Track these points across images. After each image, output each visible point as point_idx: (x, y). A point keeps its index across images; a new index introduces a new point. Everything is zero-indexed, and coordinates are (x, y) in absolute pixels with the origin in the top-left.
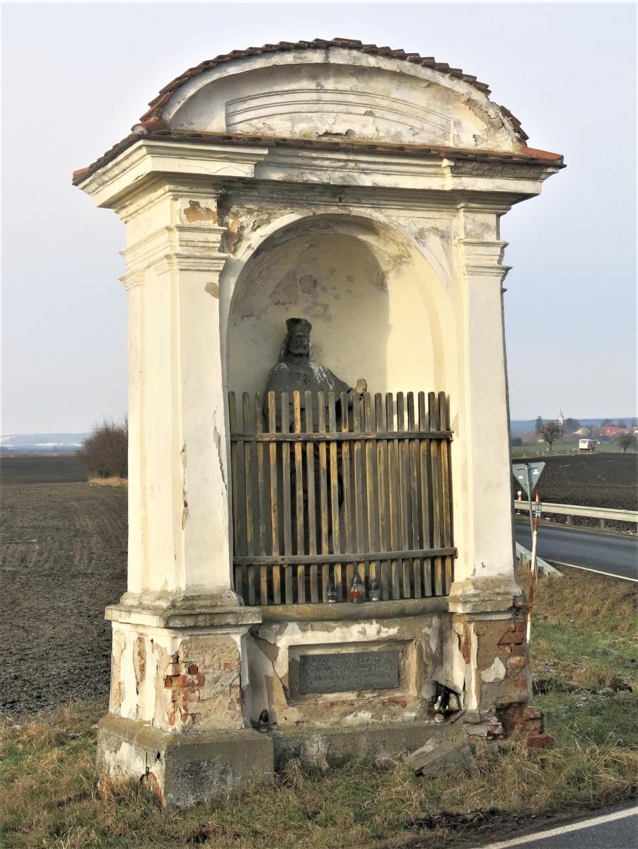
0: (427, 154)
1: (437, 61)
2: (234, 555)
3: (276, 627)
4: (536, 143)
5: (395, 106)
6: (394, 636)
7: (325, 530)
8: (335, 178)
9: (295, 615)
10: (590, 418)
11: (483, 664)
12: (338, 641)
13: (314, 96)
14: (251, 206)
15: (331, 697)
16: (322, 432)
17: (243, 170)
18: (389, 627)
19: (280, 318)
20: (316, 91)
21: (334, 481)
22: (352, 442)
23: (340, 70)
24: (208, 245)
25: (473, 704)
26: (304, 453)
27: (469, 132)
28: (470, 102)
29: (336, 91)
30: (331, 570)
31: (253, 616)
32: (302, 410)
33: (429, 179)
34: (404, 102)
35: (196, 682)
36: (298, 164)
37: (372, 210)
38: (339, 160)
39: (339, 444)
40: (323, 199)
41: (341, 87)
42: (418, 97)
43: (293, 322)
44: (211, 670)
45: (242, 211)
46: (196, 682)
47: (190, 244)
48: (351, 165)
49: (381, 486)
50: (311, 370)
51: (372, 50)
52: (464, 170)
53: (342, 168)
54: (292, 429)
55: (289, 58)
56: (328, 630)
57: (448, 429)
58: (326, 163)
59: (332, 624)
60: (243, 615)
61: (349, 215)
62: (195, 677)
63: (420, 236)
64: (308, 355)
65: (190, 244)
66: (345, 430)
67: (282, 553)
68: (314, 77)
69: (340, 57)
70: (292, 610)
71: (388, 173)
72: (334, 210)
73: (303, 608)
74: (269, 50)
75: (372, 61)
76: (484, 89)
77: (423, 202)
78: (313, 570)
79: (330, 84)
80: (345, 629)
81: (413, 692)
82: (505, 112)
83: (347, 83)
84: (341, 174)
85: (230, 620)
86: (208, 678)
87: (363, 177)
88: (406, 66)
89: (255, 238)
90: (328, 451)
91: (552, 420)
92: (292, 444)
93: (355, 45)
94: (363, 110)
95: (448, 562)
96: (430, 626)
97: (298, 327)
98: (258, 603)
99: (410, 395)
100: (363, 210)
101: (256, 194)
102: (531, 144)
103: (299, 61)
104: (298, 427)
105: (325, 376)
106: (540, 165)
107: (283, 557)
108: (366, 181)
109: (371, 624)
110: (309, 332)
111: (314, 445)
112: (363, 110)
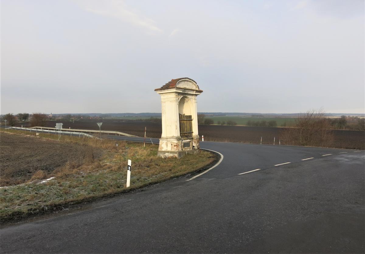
0: (194, 90)
4: (201, 89)
10: (208, 112)
11: (197, 144)
23: (188, 81)
25: (196, 148)
27: (194, 88)
28: (195, 85)
33: (166, 96)
42: (191, 84)
63: (191, 99)
69: (187, 79)
76: (196, 83)
79: (185, 82)
81: (191, 147)
82: (198, 86)
83: (186, 82)
89: (180, 98)
102: (200, 89)
106: (201, 92)
108: (189, 93)
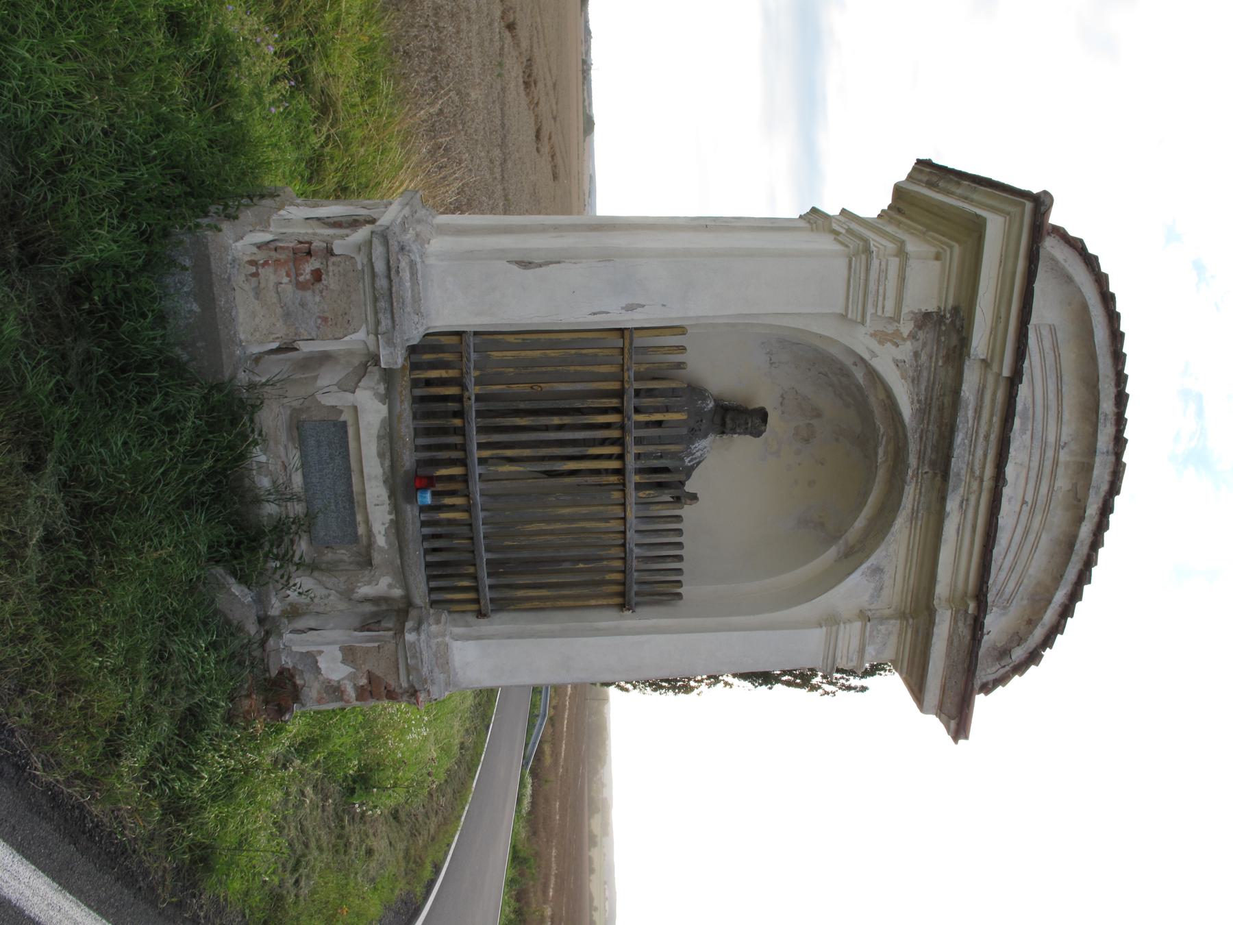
1: (1086, 588)
2: (476, 333)
3: (382, 388)
5: (1032, 537)
6: (375, 542)
7: (509, 453)
9: (398, 409)
12: (365, 470)
13: (1051, 438)
14: (924, 357)
16: (633, 450)
17: (979, 342)
18: (386, 535)
19: (765, 398)
20: (1058, 439)
21: (572, 466)
22: (622, 487)
24: (881, 298)
26: (607, 426)
29: (1056, 463)
31: (393, 357)
32: (659, 424)
34: (1035, 547)
35: (301, 279)
36: (980, 417)
37: (910, 511)
38: (983, 468)
39: (620, 472)
40: (929, 450)
41: (1061, 470)
43: (763, 415)
44: (317, 299)
45: (918, 345)
46: (301, 279)
47: (883, 274)
48: (975, 485)
50: (705, 437)
52: (960, 624)
53: (972, 472)
54: (637, 410)
55: (1107, 406)
56: (381, 455)
57: (637, 604)
58: (979, 453)
59: (387, 463)
60: (390, 343)
61: (904, 482)
62: (308, 277)
64: (723, 433)
65: (883, 274)
67: (479, 398)
70: (405, 408)
71: (959, 531)
73: (406, 427)
75: (1092, 510)
78: (456, 440)
80: (381, 478)
84: (963, 472)
85: (383, 324)
86: (308, 294)
87: (958, 500)
88: (1081, 549)
90: (609, 457)
91: (629, 620)
92: (618, 410)
93: (1114, 488)
94: (1029, 498)
95: (474, 607)
96: (390, 586)
97: (758, 421)
98: (415, 366)
100: (911, 497)
101: (940, 363)
103: (1101, 417)
104: (642, 418)
105: (698, 454)
107: (473, 398)
108: (952, 505)
109: (390, 513)
110: (751, 434)
111: (619, 439)
112: (1029, 498)
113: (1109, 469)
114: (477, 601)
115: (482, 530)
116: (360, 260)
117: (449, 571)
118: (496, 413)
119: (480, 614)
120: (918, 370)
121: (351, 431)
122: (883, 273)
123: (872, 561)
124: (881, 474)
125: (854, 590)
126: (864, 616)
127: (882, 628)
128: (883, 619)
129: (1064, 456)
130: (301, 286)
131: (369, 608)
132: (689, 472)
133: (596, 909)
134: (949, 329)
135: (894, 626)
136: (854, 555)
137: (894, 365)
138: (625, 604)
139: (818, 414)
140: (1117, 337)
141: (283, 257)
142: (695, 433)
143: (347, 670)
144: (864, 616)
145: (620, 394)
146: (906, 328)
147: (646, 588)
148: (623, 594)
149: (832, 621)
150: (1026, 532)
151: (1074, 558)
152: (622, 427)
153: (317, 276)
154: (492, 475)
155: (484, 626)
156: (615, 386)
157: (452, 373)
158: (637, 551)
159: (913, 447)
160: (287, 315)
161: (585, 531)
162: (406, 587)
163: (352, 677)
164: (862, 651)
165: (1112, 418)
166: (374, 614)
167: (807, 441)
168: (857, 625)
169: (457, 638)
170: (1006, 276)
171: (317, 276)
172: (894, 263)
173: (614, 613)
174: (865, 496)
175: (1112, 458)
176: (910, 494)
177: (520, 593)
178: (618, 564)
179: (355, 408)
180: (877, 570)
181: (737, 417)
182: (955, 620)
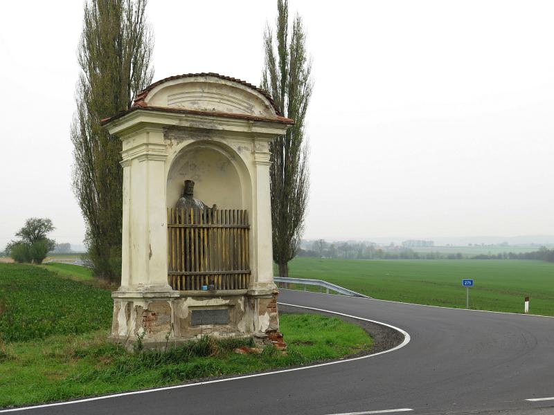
1: (247, 82)
8: (208, 126)
15: (204, 327)
29: (208, 93)
30: (205, 278)
41: (210, 91)
43: (187, 182)
49: (221, 243)
51: (223, 78)
55: (192, 80)
66: (210, 224)
67: (186, 271)
68: (201, 87)
72: (206, 139)
74: (184, 76)
75: (223, 82)
77: (127, 121)
88: (235, 85)
91: (253, 227)
93: (217, 76)
95: (248, 276)
99: (234, 211)
108: (220, 128)
112: (218, 100)
113: (211, 78)
114: (246, 274)
115: (224, 271)
116: (150, 301)
117: (236, 282)
118: (188, 265)
119: (250, 274)
120: (179, 138)
121: (195, 309)
122: (153, 150)
123: (236, 150)
124: (209, 146)
125: (246, 156)
126: (253, 153)
127: (257, 147)
128: (255, 146)
129: (206, 90)
130: (156, 319)
131: (247, 308)
132: (206, 207)
133: (392, 244)
134: (168, 130)
135: (256, 143)
136: (234, 156)
137: (177, 147)
138: (247, 228)
139: (187, 163)
140: (172, 78)
141: (148, 324)
142: (193, 205)
143: (266, 314)
144: (253, 153)
145: (180, 228)
146: (169, 142)
147: (243, 221)
148: (245, 229)
149: (254, 163)
150: (228, 100)
151: (238, 87)
152: (190, 228)
153: (154, 314)
154: (206, 266)
155: (253, 273)
156: (178, 230)
157: (179, 278)
158: (236, 224)
159: (202, 139)
160: (164, 323)
161: (225, 240)
162: (241, 295)
163: (269, 313)
164: (264, 153)
165: (195, 78)
166: (249, 306)
167: (195, 166)
168: (256, 155)
169: (257, 281)
170: (157, 116)
171: (154, 314)
172: (150, 147)
173: (250, 232)
174: (214, 151)
175: (207, 77)
176: (216, 139)
177: (244, 261)
178: (235, 230)
179: (189, 307)
180: (239, 149)
181: (187, 190)
182: (255, 126)
